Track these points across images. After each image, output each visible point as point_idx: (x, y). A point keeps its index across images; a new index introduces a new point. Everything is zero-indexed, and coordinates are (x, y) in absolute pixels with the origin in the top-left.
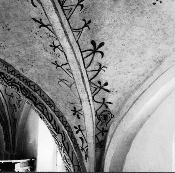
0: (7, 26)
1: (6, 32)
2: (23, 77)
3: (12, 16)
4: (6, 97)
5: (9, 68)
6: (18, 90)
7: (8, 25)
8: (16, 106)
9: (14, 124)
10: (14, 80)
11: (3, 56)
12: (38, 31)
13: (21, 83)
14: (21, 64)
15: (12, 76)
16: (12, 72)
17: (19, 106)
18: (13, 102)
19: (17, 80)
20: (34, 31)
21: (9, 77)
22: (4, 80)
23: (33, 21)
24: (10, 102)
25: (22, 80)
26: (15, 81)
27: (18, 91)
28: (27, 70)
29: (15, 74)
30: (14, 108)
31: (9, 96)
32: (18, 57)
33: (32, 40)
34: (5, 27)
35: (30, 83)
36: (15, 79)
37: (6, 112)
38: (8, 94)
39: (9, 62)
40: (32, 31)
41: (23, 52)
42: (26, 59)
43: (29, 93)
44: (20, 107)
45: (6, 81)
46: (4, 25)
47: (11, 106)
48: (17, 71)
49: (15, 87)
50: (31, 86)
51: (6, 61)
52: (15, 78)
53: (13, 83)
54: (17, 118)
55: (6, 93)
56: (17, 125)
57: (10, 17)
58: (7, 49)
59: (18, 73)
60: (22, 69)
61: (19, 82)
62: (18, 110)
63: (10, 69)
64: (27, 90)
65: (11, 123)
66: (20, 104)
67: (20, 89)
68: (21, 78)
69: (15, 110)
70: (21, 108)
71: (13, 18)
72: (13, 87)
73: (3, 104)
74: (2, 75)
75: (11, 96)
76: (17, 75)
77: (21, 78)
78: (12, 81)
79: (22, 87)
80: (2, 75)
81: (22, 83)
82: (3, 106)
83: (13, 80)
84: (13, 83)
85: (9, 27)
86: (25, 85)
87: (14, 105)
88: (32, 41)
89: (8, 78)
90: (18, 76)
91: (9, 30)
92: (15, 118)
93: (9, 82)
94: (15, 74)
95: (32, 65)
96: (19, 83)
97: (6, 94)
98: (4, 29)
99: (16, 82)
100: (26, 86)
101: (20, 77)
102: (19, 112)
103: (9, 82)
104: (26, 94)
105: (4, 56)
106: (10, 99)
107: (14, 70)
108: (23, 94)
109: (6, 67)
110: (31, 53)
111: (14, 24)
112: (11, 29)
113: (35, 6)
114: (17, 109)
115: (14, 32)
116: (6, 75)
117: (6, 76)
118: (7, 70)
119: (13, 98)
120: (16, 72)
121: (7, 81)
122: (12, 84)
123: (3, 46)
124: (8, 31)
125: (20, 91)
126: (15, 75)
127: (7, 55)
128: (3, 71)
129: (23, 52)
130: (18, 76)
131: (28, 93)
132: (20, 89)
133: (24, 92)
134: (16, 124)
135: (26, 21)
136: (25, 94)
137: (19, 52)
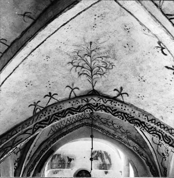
0: (142, 78)
1: (142, 84)
2: (164, 125)
3: (146, 68)
4: (154, 145)
5: (149, 117)
6: (160, 138)
7: (143, 77)
8: (165, 154)
9: (164, 173)
10: (155, 129)
11: (142, 106)
12: (172, 78)
13: (162, 131)
14: (160, 112)
15: (152, 125)
16: (152, 120)
17: (168, 155)
18: (161, 151)
19: (158, 128)
20: (168, 79)
21: (150, 125)
22: (145, 129)
23: (167, 69)
24: (158, 150)
25: (163, 128)
26: (156, 129)
27: (160, 139)
28: (167, 118)
29: (155, 122)
30: (164, 157)
31: (157, 144)
32: (156, 105)
33: (167, 88)
34: (140, 79)
35: (171, 130)
36: (156, 127)
37: (156, 160)
38: (155, 142)
39: (148, 110)
40: (166, 79)
41: (161, 100)
42: (164, 107)
43: (172, 141)
44: (169, 155)
45: (147, 129)
46: (140, 77)
47: (160, 154)
48: (157, 119)
49: (156, 136)
50: (173, 133)
51: (145, 110)
52: (156, 126)
53: (155, 132)
54: (167, 167)
55: (153, 141)
56: (168, 174)
57: (144, 70)
58: (145, 99)
59: (158, 121)
60: (162, 117)
61: (160, 130)
62: (167, 159)
63: (150, 118)
64: (169, 138)
65: (162, 172)
66: (169, 153)
67: (161, 137)
68: (162, 126)
69: (164, 159)
70: (170, 156)
71: (147, 70)
72: (155, 136)
73: (151, 153)
74: (142, 124)
75: (158, 145)
76: (157, 123)
77: (162, 126)
78: (153, 129)
79: (164, 135)
80: (142, 124)
81: (164, 131)
82: (152, 155)
83: (154, 129)
84: (155, 132)
85: (144, 79)
86: (166, 133)
87: (163, 154)
88: (168, 88)
89: (149, 126)
90: (159, 124)
91: (144, 81)
92: (165, 167)
93: (150, 130)
94: (155, 122)
95: (171, 112)
96: (161, 131)
97: (154, 142)
98: (140, 81)
99: (157, 130)
100: (168, 134)
101: (161, 125)
102: (168, 161)
103: (150, 130)
104: (169, 142)
105: (143, 106)
106: (158, 148)
107: (154, 118)
108: (166, 143)
109: (145, 116)
110: (169, 100)
111: (148, 75)
112: (146, 80)
113: (166, 55)
114: (166, 158)
115: (149, 82)
116: (147, 124)
117: (147, 125)
118: (147, 119)
119: (161, 146)
120: (156, 120)
121: (149, 130)
122: (153, 132)
123: (141, 97)
124: (144, 82)
125: (162, 139)
126: (156, 123)
127: (146, 105)
128: (144, 120)
129: (161, 100)
130: (159, 124)
131: (170, 141)
132: (161, 137)
133: (167, 140)
134: (166, 173)
135: (159, 70)
136: (167, 142)
137: (157, 101)
